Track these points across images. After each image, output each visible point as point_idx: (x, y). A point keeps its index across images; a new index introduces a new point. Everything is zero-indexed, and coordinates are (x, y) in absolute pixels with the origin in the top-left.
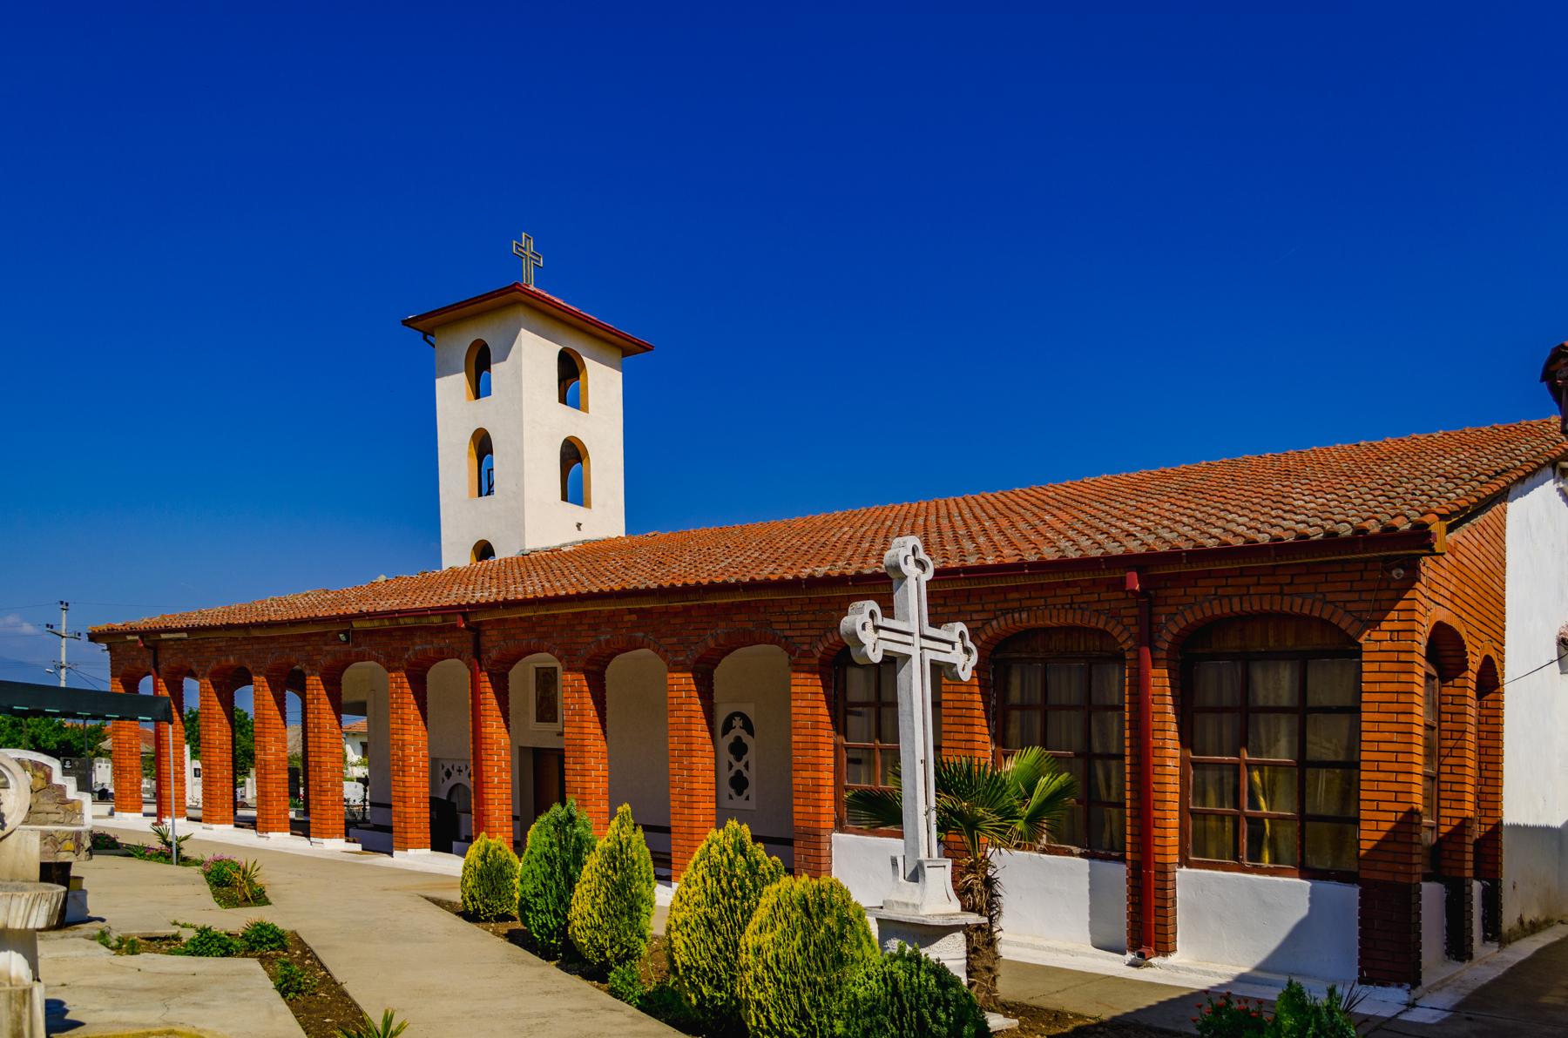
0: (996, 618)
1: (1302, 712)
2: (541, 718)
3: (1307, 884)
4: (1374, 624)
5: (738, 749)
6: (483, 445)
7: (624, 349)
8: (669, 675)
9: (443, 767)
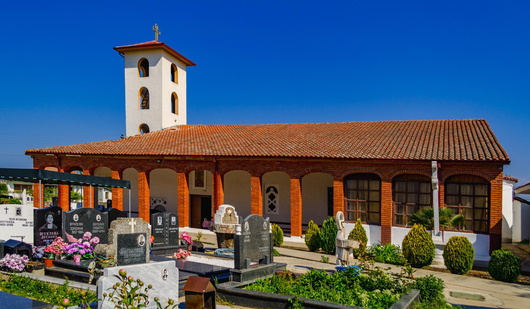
0: (398, 171)
1: (474, 196)
2: (197, 185)
3: (476, 235)
4: (494, 179)
5: (272, 197)
6: (145, 93)
7: (188, 64)
8: (291, 179)
9: (153, 200)
